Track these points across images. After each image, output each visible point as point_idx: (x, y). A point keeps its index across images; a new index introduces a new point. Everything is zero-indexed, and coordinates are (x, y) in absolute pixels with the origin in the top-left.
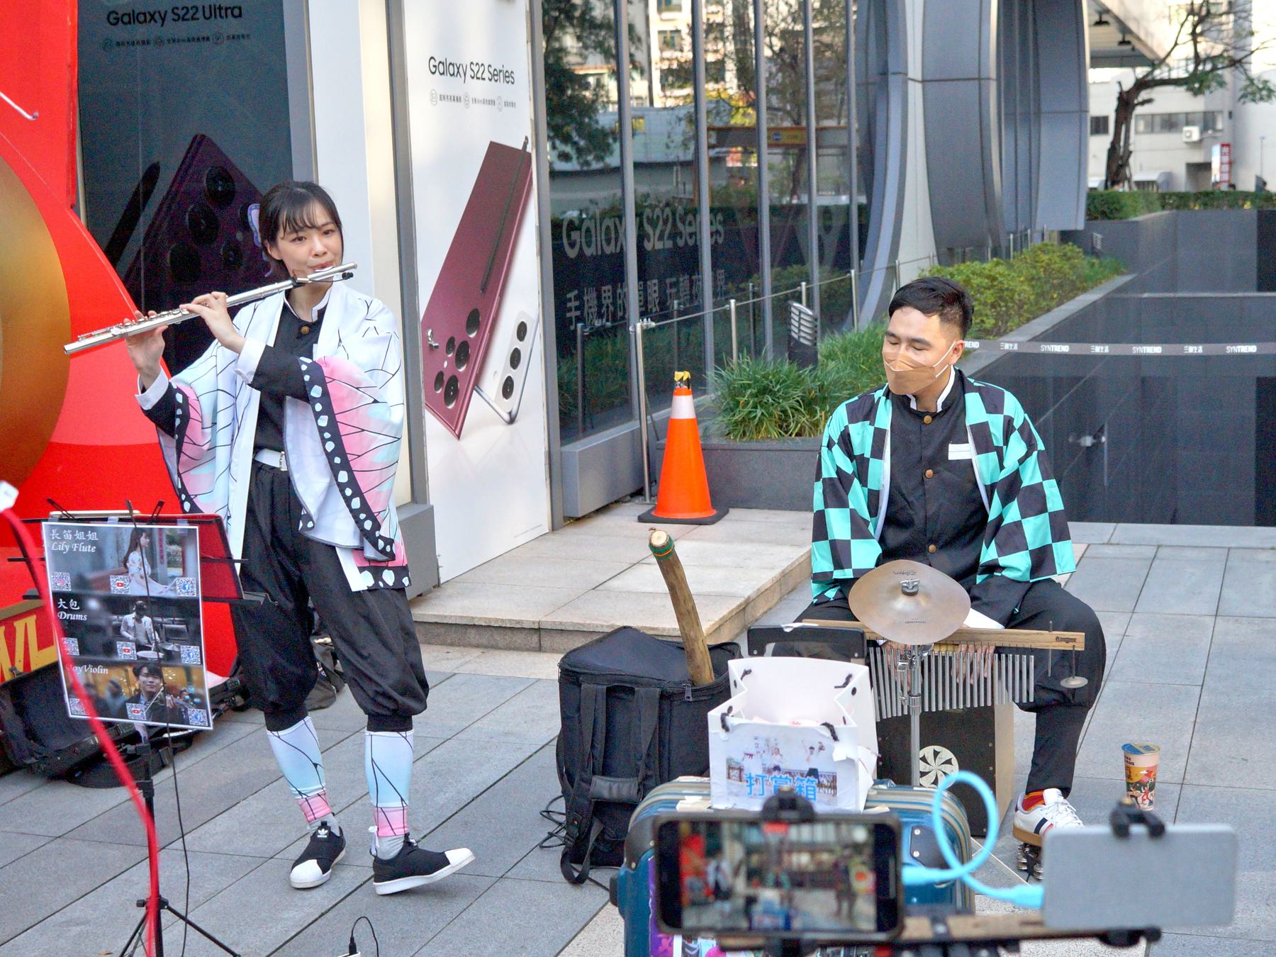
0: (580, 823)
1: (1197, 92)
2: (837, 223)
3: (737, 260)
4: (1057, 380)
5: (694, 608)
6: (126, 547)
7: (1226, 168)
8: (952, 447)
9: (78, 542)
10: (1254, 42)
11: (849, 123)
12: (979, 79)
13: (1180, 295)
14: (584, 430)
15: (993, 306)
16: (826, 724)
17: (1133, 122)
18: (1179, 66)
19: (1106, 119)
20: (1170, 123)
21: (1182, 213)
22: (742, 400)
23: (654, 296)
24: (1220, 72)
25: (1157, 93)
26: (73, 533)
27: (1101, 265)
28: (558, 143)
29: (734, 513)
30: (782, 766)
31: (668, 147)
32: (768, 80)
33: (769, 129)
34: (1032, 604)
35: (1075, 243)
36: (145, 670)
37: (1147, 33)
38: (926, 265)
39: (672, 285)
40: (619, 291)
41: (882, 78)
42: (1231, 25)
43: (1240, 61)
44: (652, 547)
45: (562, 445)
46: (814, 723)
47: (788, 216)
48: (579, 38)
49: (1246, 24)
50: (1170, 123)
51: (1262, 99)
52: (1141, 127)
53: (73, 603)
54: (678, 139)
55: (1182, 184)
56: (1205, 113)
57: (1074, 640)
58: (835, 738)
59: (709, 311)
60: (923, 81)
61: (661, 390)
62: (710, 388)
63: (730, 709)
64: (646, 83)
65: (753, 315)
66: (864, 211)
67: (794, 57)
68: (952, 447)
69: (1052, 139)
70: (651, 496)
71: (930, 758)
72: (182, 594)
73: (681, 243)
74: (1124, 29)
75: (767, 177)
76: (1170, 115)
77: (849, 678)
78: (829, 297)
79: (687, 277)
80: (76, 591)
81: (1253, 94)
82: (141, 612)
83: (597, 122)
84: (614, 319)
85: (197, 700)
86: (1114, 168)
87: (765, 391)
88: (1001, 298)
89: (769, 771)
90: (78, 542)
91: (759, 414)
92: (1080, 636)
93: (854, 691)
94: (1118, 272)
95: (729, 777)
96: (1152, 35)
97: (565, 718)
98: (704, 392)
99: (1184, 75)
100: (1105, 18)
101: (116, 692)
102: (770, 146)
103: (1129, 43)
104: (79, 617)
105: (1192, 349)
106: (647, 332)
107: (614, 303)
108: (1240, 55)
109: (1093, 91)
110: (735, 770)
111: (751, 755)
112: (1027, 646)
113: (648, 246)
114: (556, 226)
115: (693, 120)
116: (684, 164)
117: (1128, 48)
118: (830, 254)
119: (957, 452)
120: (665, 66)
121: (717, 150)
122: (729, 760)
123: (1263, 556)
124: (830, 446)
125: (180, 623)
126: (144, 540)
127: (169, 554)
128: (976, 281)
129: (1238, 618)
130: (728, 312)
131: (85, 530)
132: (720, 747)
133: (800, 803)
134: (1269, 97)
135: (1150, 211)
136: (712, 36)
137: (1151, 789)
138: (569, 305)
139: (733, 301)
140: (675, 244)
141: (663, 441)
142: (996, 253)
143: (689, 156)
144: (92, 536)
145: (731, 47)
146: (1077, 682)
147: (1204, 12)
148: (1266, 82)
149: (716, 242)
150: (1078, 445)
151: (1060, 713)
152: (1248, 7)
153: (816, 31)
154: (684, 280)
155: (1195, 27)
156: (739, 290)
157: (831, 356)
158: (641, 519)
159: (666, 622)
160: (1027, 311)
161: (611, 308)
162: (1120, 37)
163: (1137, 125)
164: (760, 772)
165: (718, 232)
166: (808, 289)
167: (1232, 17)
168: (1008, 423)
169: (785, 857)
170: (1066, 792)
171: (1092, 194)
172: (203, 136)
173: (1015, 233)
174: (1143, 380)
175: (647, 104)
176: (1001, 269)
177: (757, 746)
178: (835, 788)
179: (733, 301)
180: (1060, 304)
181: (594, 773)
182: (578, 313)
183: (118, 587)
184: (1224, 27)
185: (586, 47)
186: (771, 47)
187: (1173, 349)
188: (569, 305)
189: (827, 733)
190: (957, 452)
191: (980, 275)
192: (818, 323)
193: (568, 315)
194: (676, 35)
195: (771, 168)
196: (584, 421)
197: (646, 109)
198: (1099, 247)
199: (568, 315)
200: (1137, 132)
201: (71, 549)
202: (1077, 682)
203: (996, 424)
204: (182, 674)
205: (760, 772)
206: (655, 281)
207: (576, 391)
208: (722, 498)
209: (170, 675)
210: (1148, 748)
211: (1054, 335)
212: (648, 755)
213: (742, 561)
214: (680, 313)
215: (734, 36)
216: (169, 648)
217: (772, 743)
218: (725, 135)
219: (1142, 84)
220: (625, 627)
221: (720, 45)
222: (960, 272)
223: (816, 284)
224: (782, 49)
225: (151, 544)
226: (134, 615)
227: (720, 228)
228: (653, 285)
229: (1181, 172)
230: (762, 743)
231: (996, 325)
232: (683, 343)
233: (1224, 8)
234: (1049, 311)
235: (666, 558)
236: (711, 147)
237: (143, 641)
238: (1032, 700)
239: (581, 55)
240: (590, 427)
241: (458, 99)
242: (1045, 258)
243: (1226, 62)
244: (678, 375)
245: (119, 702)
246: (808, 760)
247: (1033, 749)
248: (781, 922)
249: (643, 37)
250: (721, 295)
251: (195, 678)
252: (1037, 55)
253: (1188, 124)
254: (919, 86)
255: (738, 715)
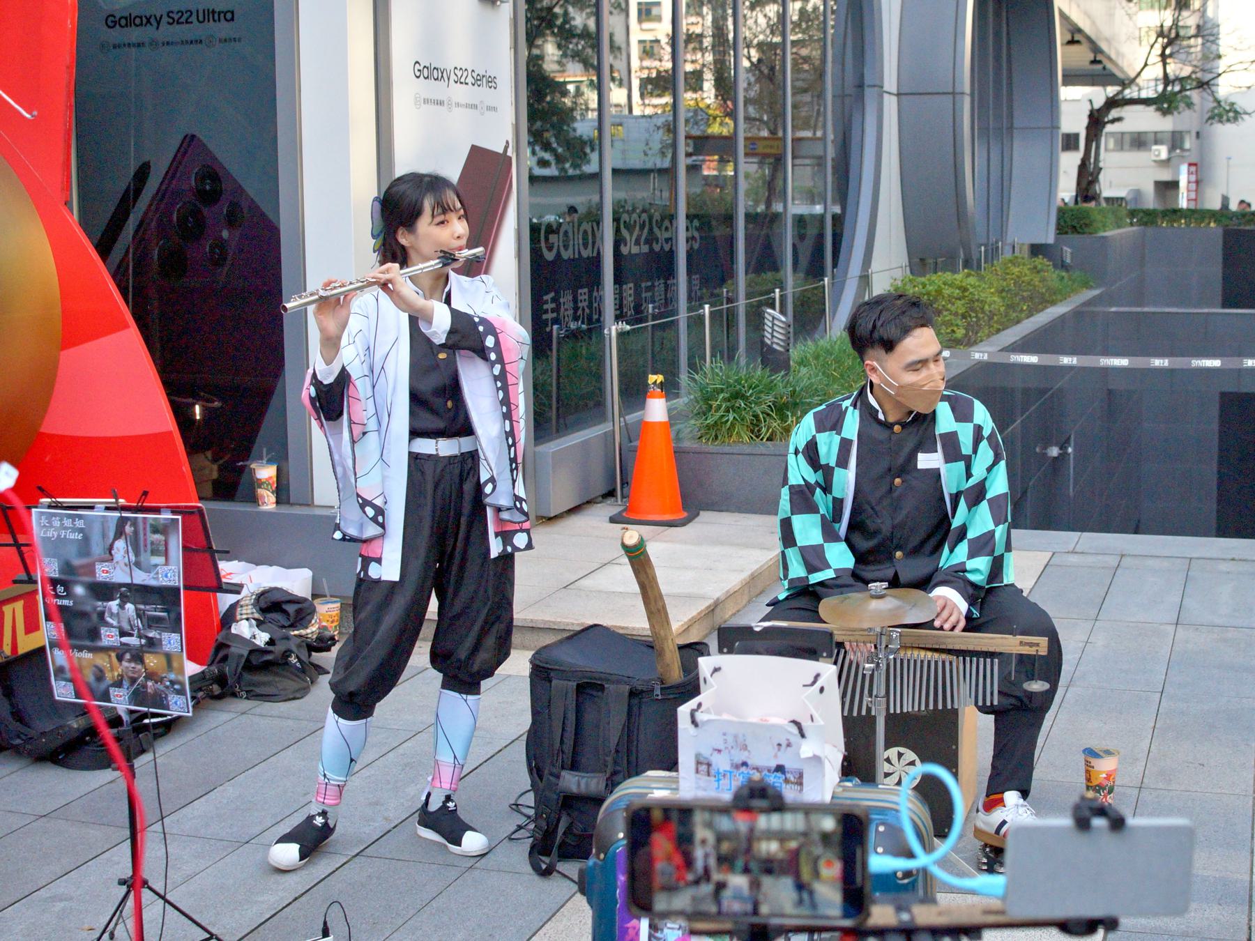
0: (548, 817)
1: (1165, 113)
2: (812, 232)
3: (712, 267)
4: (1026, 391)
5: (664, 607)
6: (111, 535)
7: (1193, 186)
8: (921, 456)
9: (66, 528)
10: (1222, 65)
11: (825, 133)
12: (953, 93)
13: (1146, 309)
14: (558, 431)
15: (964, 316)
16: (794, 722)
17: (1103, 139)
18: (1148, 85)
19: (1077, 136)
20: (1139, 141)
21: (1150, 231)
22: (715, 404)
23: (629, 300)
24: (1188, 93)
25: (1127, 112)
26: (61, 520)
27: (1070, 279)
28: (537, 148)
29: (705, 516)
30: (749, 762)
31: (646, 154)
32: (746, 90)
33: (746, 139)
34: (990, 605)
35: (1045, 256)
36: (128, 656)
37: (1118, 53)
38: (898, 274)
39: (648, 289)
40: (595, 294)
41: (858, 90)
42: (1199, 48)
43: (1207, 83)
44: (624, 546)
45: (536, 445)
46: (782, 721)
47: (764, 223)
48: (559, 47)
49: (1214, 47)
50: (1139, 141)
51: (1228, 120)
52: (1111, 144)
53: (60, 589)
54: (656, 146)
55: (1150, 201)
56: (1173, 133)
57: (1038, 645)
58: (803, 736)
59: (683, 315)
60: (898, 95)
61: (634, 393)
62: (683, 391)
63: (700, 705)
64: (624, 92)
65: (726, 321)
66: (838, 220)
67: (772, 69)
68: (921, 456)
69: (1024, 154)
70: (623, 497)
71: (894, 759)
72: (164, 582)
73: (657, 248)
74: (1096, 49)
75: (743, 186)
76: (1139, 133)
77: (817, 677)
78: (802, 305)
79: (662, 281)
80: (63, 577)
81: (1220, 116)
82: (124, 600)
83: (574, 130)
84: (590, 321)
85: (176, 687)
86: (1084, 184)
87: (737, 395)
88: (972, 309)
89: (737, 767)
90: (66, 528)
91: (731, 419)
92: (1043, 641)
93: (822, 690)
94: (1086, 285)
95: (697, 771)
96: (1123, 56)
97: (535, 713)
98: (677, 396)
99: (1152, 94)
100: (1077, 37)
101: (100, 676)
102: (746, 155)
103: (1100, 62)
104: (66, 602)
105: (1158, 362)
106: (621, 335)
107: (590, 306)
108: (1207, 77)
109: (1064, 108)
110: (703, 765)
111: (719, 751)
112: (992, 649)
113: (624, 250)
114: (534, 229)
115: (671, 128)
116: (661, 172)
117: (1099, 67)
118: (804, 262)
119: (926, 461)
120: (645, 74)
121: (694, 158)
122: (698, 756)
123: (1223, 567)
124: (796, 452)
125: (163, 610)
126: (129, 529)
127: (152, 543)
128: (947, 291)
129: (1197, 626)
130: (701, 317)
131: (73, 517)
132: (689, 742)
133: (770, 792)
134: (1236, 119)
135: (1119, 227)
136: (691, 46)
137: (1110, 791)
138: (545, 307)
139: (707, 306)
140: (651, 250)
141: (636, 443)
142: (967, 264)
143: (666, 163)
144: (80, 524)
145: (709, 57)
146: (1037, 686)
147: (1173, 35)
148: (1232, 104)
149: (692, 248)
150: (1046, 454)
151: (1019, 717)
152: (1215, 31)
153: (793, 42)
154: (659, 285)
155: (1164, 48)
156: (712, 295)
157: (803, 362)
158: (613, 520)
159: (636, 621)
160: (996, 322)
161: (587, 311)
162: (1091, 57)
163: (1107, 142)
164: (728, 768)
165: (693, 238)
166: (781, 296)
167: (1200, 40)
168: (978, 429)
169: (756, 846)
170: (1025, 794)
171: (1062, 212)
172: (193, 136)
173: (986, 246)
174: (1110, 392)
175: (626, 112)
176: (972, 280)
177: (726, 741)
178: (801, 784)
179: (707, 306)
180: (1030, 315)
181: (563, 768)
182: (555, 315)
183: (104, 573)
184: (1193, 50)
185: (565, 55)
186: (749, 58)
187: (1140, 362)
188: (545, 307)
189: (795, 730)
190: (926, 461)
191: (950, 286)
192: (791, 330)
193: (544, 317)
194: (655, 45)
195: (747, 176)
196: (557, 422)
197: (625, 117)
198: (1068, 261)
199: (544, 317)
200: (1106, 150)
201: (59, 536)
202: (1037, 686)
203: (965, 434)
204: (163, 660)
205: (728, 768)
206: (631, 285)
207: (551, 392)
208: (693, 500)
209: (152, 661)
210: (1108, 753)
211: (1024, 346)
212: (617, 751)
213: (715, 563)
214: (655, 318)
215: (713, 47)
216: (151, 635)
217: (740, 739)
218: (702, 144)
219: (1112, 103)
220: (596, 625)
221: (699, 55)
222: (932, 283)
223: (790, 291)
224: (759, 60)
225: (136, 533)
226: (117, 602)
227: (696, 234)
228: (629, 289)
229: (1149, 189)
230: (730, 739)
231: (966, 335)
232: (657, 348)
233: (1192, 31)
234: (1018, 322)
235: (638, 557)
236: (688, 155)
237: (126, 627)
238: (996, 703)
239: (559, 63)
240: (563, 429)
241: (441, 103)
242: (1016, 270)
243: (1194, 84)
244: (652, 378)
245: (103, 686)
246: (776, 756)
247: (992, 753)
248: (749, 907)
249: (623, 46)
250: (695, 300)
251: (175, 664)
252: (1010, 78)
253: (1156, 143)
254: (894, 99)
255: (708, 711)
